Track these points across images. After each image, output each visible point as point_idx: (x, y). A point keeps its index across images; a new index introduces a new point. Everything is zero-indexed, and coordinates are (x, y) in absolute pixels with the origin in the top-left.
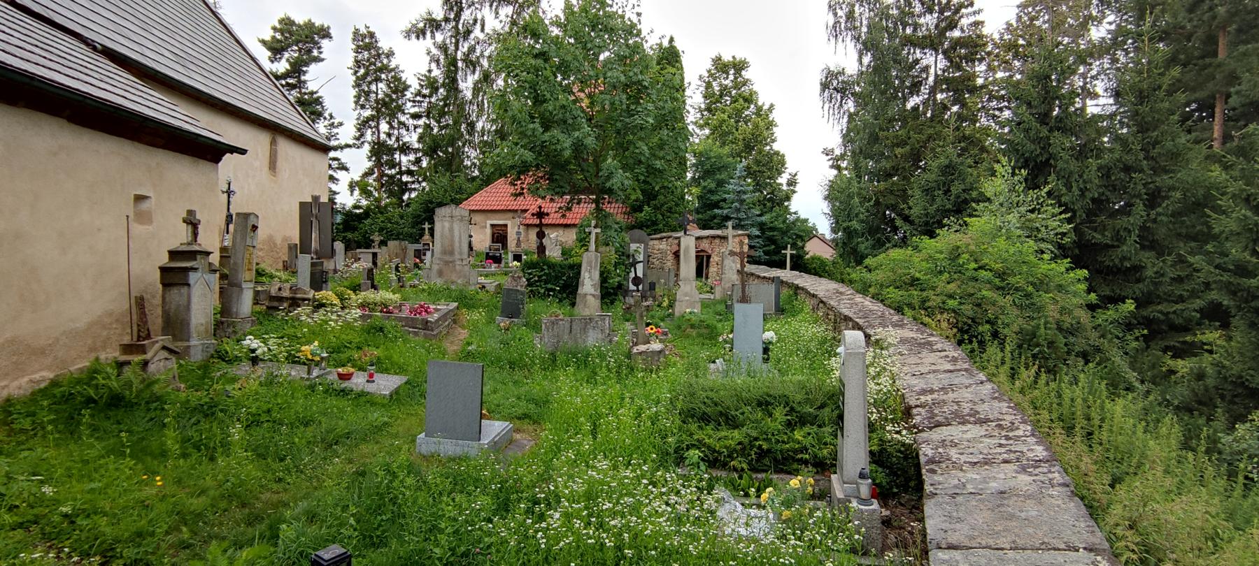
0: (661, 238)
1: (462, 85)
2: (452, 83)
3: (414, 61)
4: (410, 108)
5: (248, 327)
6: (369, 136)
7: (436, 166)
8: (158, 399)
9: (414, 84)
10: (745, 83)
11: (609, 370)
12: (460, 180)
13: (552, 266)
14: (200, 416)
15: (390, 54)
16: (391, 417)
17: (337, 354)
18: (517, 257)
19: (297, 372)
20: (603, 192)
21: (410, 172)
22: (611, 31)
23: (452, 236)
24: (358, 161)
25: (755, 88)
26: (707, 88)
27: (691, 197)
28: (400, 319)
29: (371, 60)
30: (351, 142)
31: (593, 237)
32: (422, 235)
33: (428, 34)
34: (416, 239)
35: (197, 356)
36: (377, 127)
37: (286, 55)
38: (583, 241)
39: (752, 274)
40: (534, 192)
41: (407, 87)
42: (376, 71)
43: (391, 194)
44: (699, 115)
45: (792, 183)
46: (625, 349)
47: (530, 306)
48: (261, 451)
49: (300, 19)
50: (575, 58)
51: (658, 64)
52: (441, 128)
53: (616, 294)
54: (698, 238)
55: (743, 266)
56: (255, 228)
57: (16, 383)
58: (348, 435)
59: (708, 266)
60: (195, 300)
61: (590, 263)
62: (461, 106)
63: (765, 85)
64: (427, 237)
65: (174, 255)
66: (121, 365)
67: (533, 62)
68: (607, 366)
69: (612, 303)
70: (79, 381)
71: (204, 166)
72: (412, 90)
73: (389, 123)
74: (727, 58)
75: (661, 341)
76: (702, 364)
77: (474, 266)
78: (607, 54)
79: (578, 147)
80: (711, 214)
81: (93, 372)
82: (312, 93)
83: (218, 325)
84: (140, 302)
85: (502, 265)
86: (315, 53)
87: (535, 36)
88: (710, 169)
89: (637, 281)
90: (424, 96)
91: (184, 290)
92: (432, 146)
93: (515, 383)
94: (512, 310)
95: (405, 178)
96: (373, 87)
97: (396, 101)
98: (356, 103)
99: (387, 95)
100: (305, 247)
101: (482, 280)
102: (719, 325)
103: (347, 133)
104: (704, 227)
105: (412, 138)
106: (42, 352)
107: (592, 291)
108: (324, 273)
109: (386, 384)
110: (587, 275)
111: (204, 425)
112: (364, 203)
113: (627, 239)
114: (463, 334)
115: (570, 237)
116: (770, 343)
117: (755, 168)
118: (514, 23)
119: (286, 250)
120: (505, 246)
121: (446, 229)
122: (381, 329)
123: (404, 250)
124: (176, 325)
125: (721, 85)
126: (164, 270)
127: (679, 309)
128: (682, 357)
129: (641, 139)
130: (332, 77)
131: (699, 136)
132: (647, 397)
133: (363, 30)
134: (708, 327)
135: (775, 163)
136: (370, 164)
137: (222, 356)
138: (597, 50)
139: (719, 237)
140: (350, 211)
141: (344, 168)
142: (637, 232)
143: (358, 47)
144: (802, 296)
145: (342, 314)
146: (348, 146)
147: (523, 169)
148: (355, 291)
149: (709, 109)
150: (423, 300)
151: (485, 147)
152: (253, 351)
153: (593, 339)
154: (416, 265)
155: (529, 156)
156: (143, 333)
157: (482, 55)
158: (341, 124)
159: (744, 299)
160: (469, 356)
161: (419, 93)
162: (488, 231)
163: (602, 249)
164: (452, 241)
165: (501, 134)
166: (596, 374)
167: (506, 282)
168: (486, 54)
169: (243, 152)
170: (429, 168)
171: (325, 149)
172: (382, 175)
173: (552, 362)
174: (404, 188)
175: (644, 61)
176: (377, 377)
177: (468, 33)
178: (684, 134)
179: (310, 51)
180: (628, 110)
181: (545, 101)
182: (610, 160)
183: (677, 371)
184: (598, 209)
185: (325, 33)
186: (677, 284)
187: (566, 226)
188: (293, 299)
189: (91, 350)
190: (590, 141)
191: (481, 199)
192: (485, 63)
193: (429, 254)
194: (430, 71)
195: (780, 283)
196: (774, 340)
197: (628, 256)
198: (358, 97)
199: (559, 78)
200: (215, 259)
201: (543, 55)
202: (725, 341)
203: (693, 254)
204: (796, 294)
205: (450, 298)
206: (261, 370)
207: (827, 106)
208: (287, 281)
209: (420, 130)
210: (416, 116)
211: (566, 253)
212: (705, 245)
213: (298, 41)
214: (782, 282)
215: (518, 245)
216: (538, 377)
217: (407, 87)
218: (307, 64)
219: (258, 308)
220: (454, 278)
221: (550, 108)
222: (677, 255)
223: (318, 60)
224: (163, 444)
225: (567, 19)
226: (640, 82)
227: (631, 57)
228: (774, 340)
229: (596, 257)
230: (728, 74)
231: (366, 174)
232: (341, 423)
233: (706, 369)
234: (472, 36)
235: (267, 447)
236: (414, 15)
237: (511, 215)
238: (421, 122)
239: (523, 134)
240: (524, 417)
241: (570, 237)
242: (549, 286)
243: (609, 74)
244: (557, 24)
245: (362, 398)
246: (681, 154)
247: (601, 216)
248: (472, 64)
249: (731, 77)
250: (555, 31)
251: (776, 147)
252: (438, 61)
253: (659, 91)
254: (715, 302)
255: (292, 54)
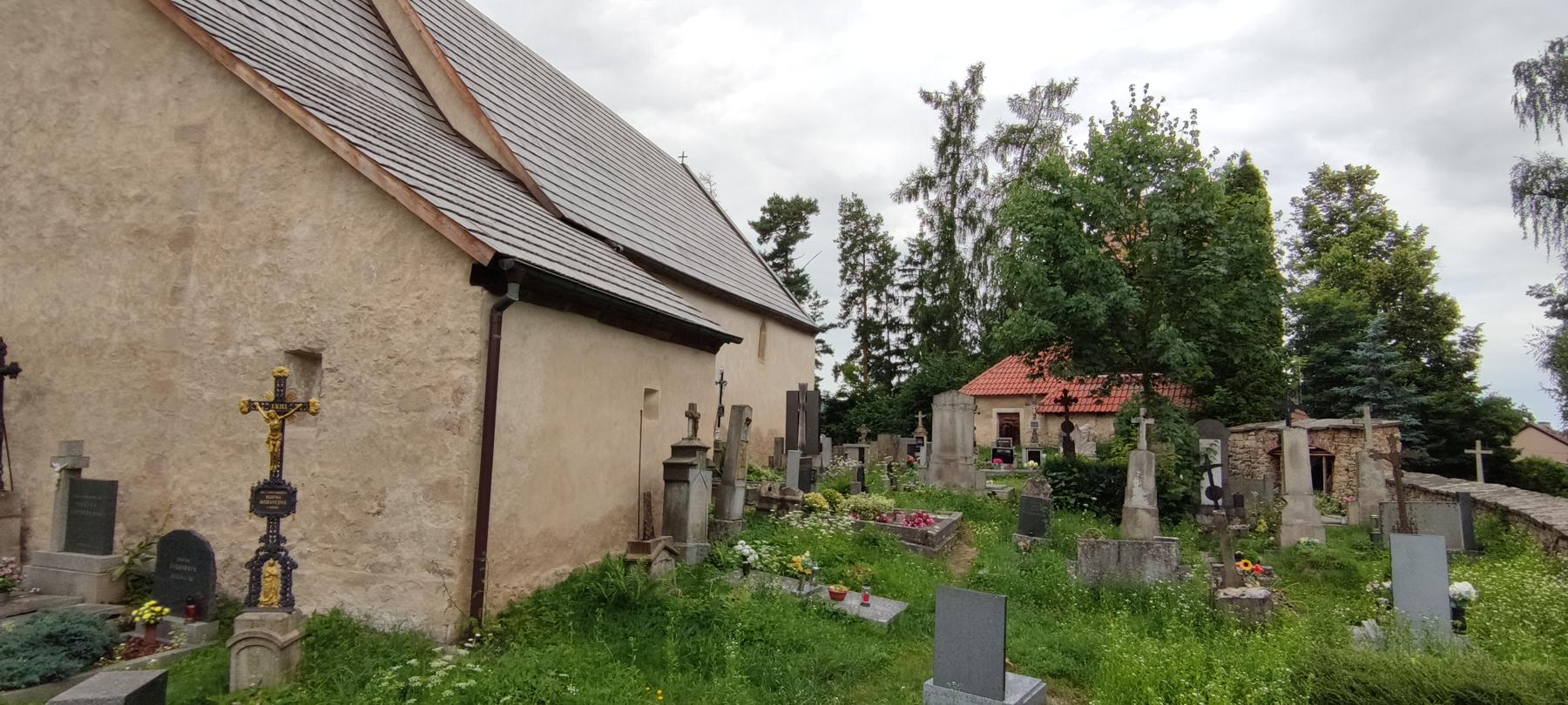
0: (1247, 431)
1: (959, 247)
2: (948, 247)
3: (904, 226)
4: (900, 279)
5: (739, 530)
6: (855, 313)
7: (929, 343)
8: (659, 603)
9: (904, 251)
10: (1372, 200)
11: (1182, 620)
12: (959, 358)
13: (1084, 468)
14: (695, 626)
15: (878, 221)
16: (890, 653)
17: (830, 568)
18: (1034, 456)
19: (789, 586)
20: (1152, 367)
21: (899, 352)
22: (1155, 160)
23: (954, 428)
24: (843, 342)
25: (1389, 207)
26: (1306, 215)
27: (1293, 370)
28: (896, 530)
29: (859, 229)
30: (836, 322)
31: (1143, 430)
32: (914, 427)
33: (921, 194)
34: (909, 430)
35: (692, 559)
36: (864, 303)
37: (774, 235)
38: (1127, 434)
39: (1414, 487)
40: (1057, 372)
41: (896, 256)
42: (863, 241)
43: (878, 378)
44: (1296, 254)
45: (1472, 341)
46: (1204, 590)
47: (1058, 521)
48: (754, 674)
49: (787, 196)
50: (1107, 200)
51: (1228, 192)
52: (935, 298)
53: (1181, 511)
54: (1311, 431)
55: (1397, 474)
56: (749, 421)
57: (544, 575)
58: (843, 669)
59: (1330, 472)
60: (692, 498)
61: (1140, 466)
62: (958, 270)
63: (1405, 197)
64: (920, 430)
65: (677, 450)
66: (628, 564)
67: (1051, 211)
68: (1179, 614)
69: (1176, 522)
70: (593, 578)
71: (705, 356)
72: (901, 258)
73: (877, 297)
74: (1337, 167)
75: (1263, 584)
76: (1338, 626)
77: (980, 466)
78: (1151, 189)
79: (1116, 314)
80: (1328, 392)
81: (604, 569)
82: (798, 272)
83: (712, 526)
84: (647, 499)
85: (1015, 465)
86: (802, 229)
87: (1053, 179)
88: (1325, 327)
89: (1213, 492)
90: (916, 264)
91: (684, 487)
92: (924, 319)
93: (1044, 624)
94: (1033, 522)
95: (894, 359)
96: (860, 259)
97: (884, 272)
98: (843, 278)
99: (874, 266)
100: (790, 441)
101: (991, 484)
102: (1362, 566)
103: (831, 313)
104: (1317, 414)
105: (902, 313)
106: (564, 545)
107: (1146, 504)
108: (812, 471)
109: (883, 610)
110: (1136, 482)
111: (700, 638)
112: (849, 389)
113: (1194, 433)
114: (971, 553)
115: (1106, 429)
116: (1465, 601)
117: (1403, 322)
118: (1025, 168)
119: (772, 444)
120: (1017, 440)
121: (947, 422)
122: (875, 542)
123: (896, 445)
124: (675, 523)
125: (1330, 208)
126: (667, 465)
127: (1286, 538)
128: (1302, 612)
129: (1207, 295)
130: (818, 253)
131: (1296, 276)
132: (1250, 669)
133: (851, 200)
134: (1341, 567)
135: (1440, 315)
136: (857, 344)
137: (714, 560)
138: (1136, 187)
139: (1346, 429)
140: (834, 400)
141: (828, 351)
142: (1209, 424)
143: (846, 218)
144: (1518, 527)
145: (834, 524)
146: (832, 326)
147: (1042, 343)
148: (844, 493)
149: (1311, 243)
150: (920, 507)
151: (986, 319)
152: (745, 558)
153: (1152, 573)
154: (910, 464)
155: (1049, 327)
156: (648, 532)
157: (984, 209)
158: (826, 302)
159: (1405, 527)
160: (980, 582)
161: (910, 261)
162: (995, 422)
163: (1157, 446)
164: (954, 434)
165: (1009, 301)
166: (1161, 624)
167: (1024, 487)
168: (989, 207)
169: (738, 340)
170: (921, 347)
171: (810, 331)
172: (869, 356)
173: (1094, 600)
174: (893, 370)
175: (1208, 194)
176: (873, 600)
177: (967, 186)
178: (1275, 283)
179: (797, 228)
180: (1185, 259)
181: (1068, 257)
182: (1162, 327)
183: (1297, 628)
184: (1148, 393)
185: (812, 207)
186: (1278, 497)
187: (1100, 414)
188: (782, 500)
189: (604, 545)
190: (1132, 303)
191: (985, 382)
192: (988, 218)
193: (923, 450)
194: (921, 235)
195: (1471, 504)
196: (1473, 596)
197: (1197, 457)
198: (844, 271)
199: (1085, 227)
200: (710, 454)
201: (1065, 203)
202: (1378, 593)
203: (1305, 455)
204: (1506, 523)
205: (952, 505)
206: (753, 580)
207: (1542, 240)
208: (774, 480)
209: (911, 303)
210: (906, 287)
211: (1103, 450)
212: (1323, 441)
213: (786, 218)
214: (1475, 501)
215: (1035, 438)
216: (1077, 619)
217: (896, 256)
218: (793, 242)
219: (748, 510)
220: (956, 479)
221: (1075, 265)
222: (1276, 455)
223: (805, 236)
224: (663, 654)
225: (1093, 154)
226: (1201, 220)
227: (1187, 189)
228: (1473, 596)
229: (1149, 459)
230: (1340, 191)
231: (851, 357)
232: (836, 653)
233: (1346, 635)
234: (972, 189)
235: (760, 672)
236: (905, 172)
237: (1023, 401)
238: (913, 293)
239: (1040, 301)
240: (1058, 675)
241: (1106, 429)
242: (1082, 495)
243: (1156, 215)
244: (1083, 163)
245: (857, 625)
246: (1273, 312)
247: (1153, 403)
248: (972, 222)
249: (1346, 196)
250: (1078, 171)
251: (1438, 289)
252: (931, 223)
253: (1232, 229)
254: (1349, 530)
255: (780, 232)
